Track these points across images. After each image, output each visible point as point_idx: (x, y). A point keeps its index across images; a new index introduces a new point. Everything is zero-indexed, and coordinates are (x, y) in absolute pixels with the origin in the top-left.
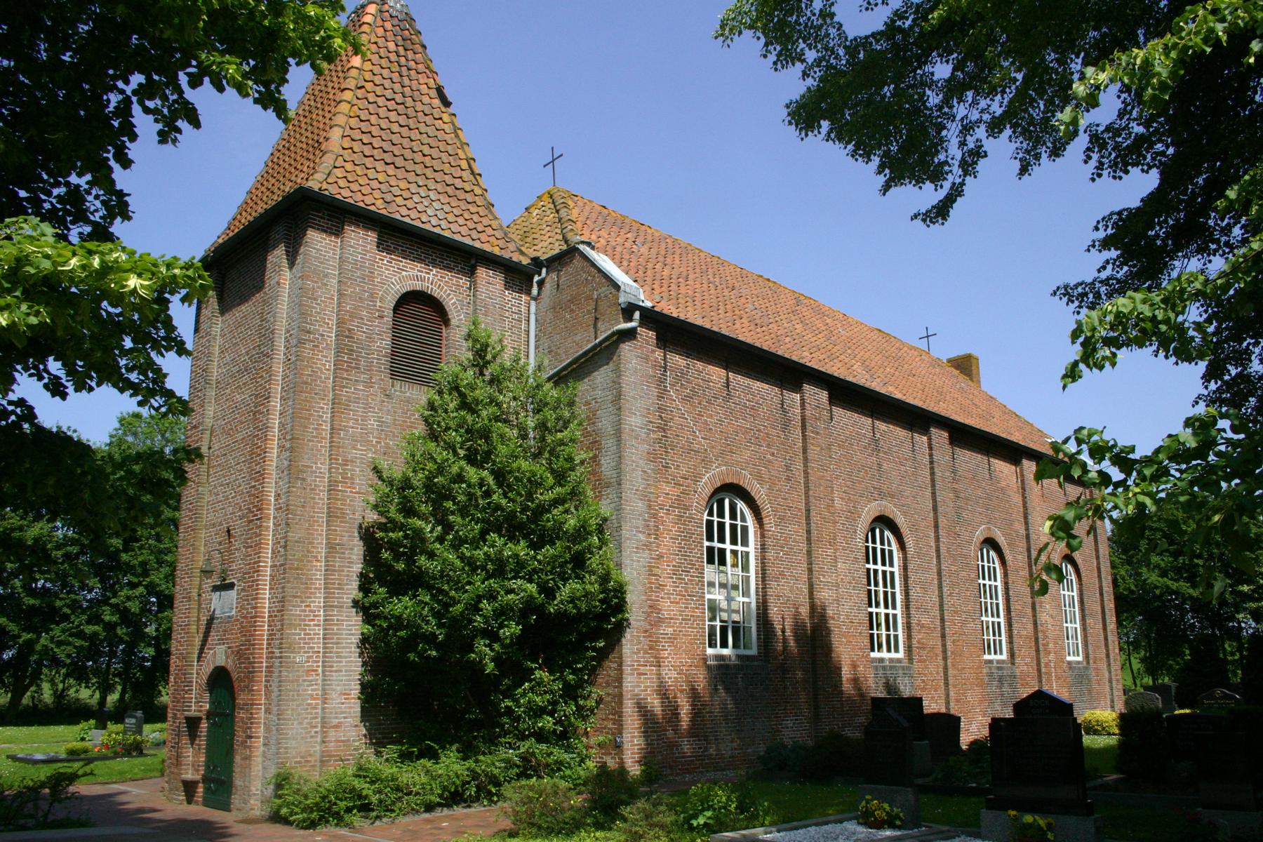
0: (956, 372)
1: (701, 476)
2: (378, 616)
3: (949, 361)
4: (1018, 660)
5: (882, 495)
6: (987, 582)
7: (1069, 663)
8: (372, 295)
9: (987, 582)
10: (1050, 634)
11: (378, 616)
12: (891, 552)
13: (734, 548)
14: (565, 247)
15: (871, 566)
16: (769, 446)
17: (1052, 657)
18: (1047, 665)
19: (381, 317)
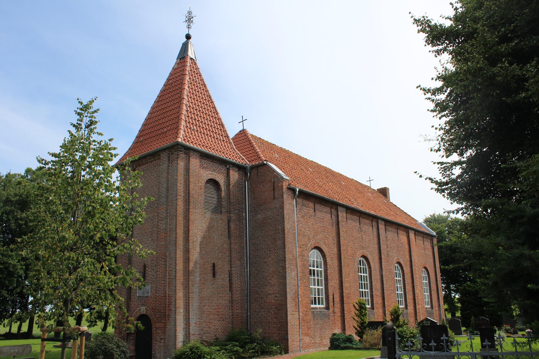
0: (381, 195)
1: (307, 244)
2: (50, 317)
3: (378, 190)
4: (408, 308)
5: (363, 248)
6: (362, 274)
7: (426, 308)
8: (199, 182)
9: (362, 274)
10: (420, 297)
11: (50, 317)
12: (366, 268)
13: (314, 268)
14: (471, 351)
15: (360, 274)
16: (328, 232)
17: (420, 306)
18: (419, 309)
19: (201, 189)
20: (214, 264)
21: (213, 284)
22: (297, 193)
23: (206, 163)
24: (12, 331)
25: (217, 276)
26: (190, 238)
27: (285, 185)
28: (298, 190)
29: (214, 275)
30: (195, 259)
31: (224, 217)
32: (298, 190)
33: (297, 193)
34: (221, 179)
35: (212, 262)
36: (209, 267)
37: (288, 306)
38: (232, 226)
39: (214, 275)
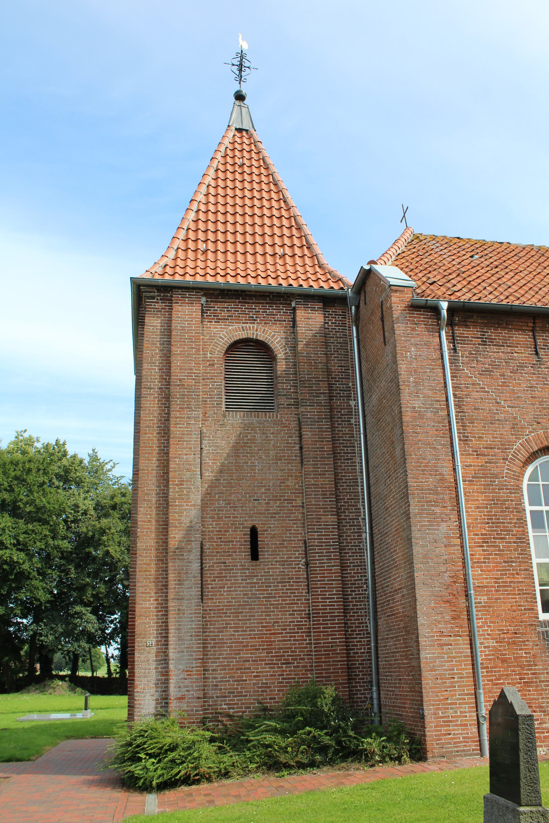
20: (254, 532)
21: (251, 577)
22: (444, 313)
23: (220, 308)
24: (83, 698)
25: (264, 555)
26: (171, 475)
27: (398, 304)
28: (444, 305)
29: (255, 555)
30: (186, 521)
31: (287, 417)
32: (444, 305)
33: (444, 313)
34: (273, 335)
35: (249, 524)
36: (241, 537)
37: (421, 620)
38: (307, 434)
39: (255, 555)
